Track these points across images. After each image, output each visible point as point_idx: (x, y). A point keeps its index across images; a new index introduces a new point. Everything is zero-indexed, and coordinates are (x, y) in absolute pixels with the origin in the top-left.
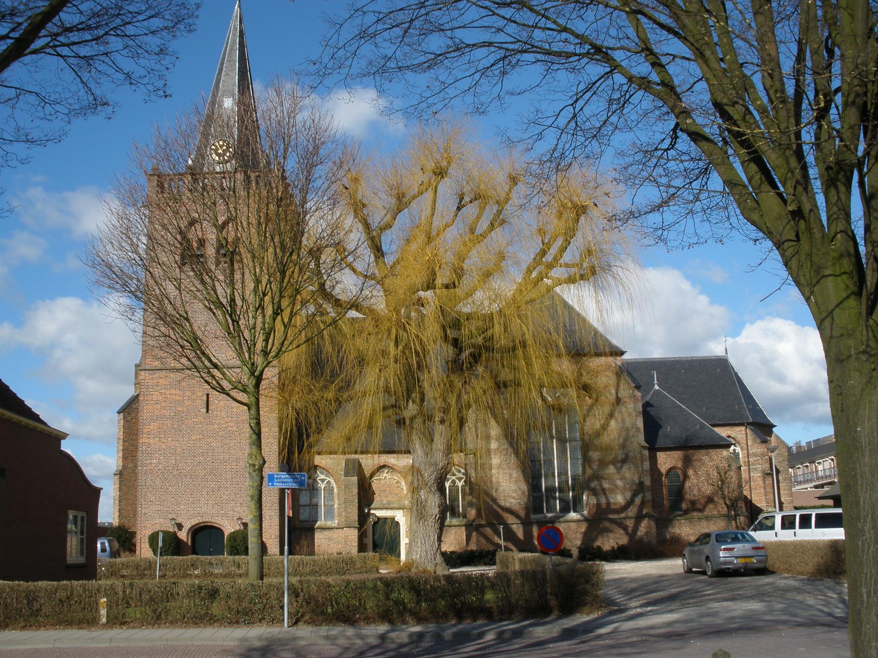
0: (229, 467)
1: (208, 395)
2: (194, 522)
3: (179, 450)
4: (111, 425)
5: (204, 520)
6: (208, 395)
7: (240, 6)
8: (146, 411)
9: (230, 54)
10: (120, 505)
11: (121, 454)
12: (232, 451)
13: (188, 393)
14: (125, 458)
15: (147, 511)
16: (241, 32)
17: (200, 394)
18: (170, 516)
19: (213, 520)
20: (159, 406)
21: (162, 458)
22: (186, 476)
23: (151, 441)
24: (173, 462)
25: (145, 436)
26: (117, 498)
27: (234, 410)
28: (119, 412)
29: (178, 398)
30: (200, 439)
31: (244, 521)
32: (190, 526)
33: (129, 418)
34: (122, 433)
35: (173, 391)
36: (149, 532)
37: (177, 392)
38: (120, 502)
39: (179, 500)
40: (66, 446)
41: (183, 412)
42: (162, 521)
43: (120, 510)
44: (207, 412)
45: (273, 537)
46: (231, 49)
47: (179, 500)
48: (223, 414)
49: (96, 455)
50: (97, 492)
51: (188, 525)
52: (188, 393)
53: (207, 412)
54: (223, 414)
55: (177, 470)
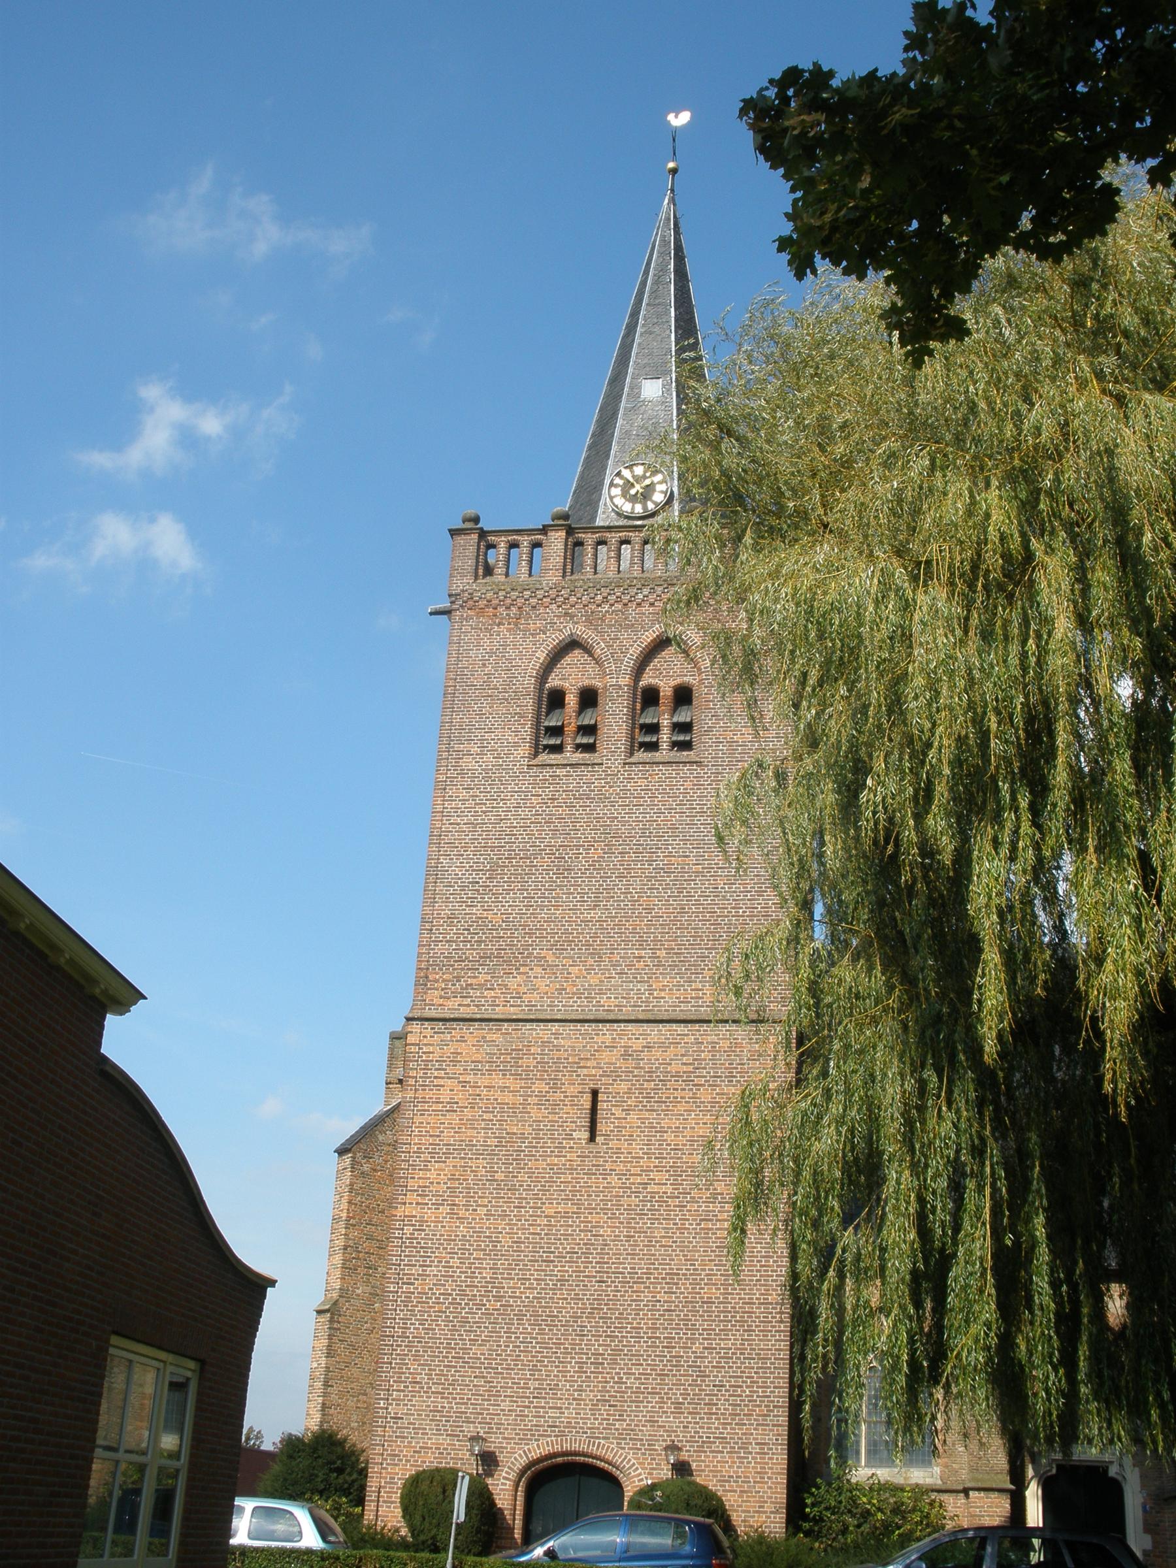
0: (646, 1297)
1: (595, 1093)
2: (539, 1448)
3: (506, 1241)
4: (323, 1187)
5: (567, 1447)
6: (595, 1093)
7: (673, 201)
8: (418, 1133)
9: (653, 292)
10: (325, 1395)
11: (338, 1259)
12: (658, 1252)
13: (540, 1086)
14: (348, 1269)
15: (402, 1410)
16: (679, 248)
17: (572, 1090)
18: (470, 1430)
19: (593, 1450)
20: (455, 1118)
21: (455, 1262)
22: (520, 1317)
23: (429, 1214)
24: (487, 1274)
25: (412, 1197)
26: (320, 1374)
27: (669, 1137)
28: (341, 1151)
29: (509, 1098)
30: (566, 1215)
31: (684, 1456)
32: (523, 1461)
33: (366, 1168)
34: (344, 1205)
35: (498, 1080)
36: (402, 1472)
37: (509, 1082)
38: (326, 1384)
39: (499, 1382)
40: (122, 1041)
41: (523, 1138)
42: (444, 1440)
43: (324, 1406)
44: (592, 1138)
45: (768, 1507)
46: (657, 282)
47: (499, 1382)
48: (637, 1148)
49: (269, 1205)
50: (254, 1288)
51: (516, 1456)
52: (540, 1086)
53: (592, 1138)
54: (637, 1148)
55: (498, 1298)
